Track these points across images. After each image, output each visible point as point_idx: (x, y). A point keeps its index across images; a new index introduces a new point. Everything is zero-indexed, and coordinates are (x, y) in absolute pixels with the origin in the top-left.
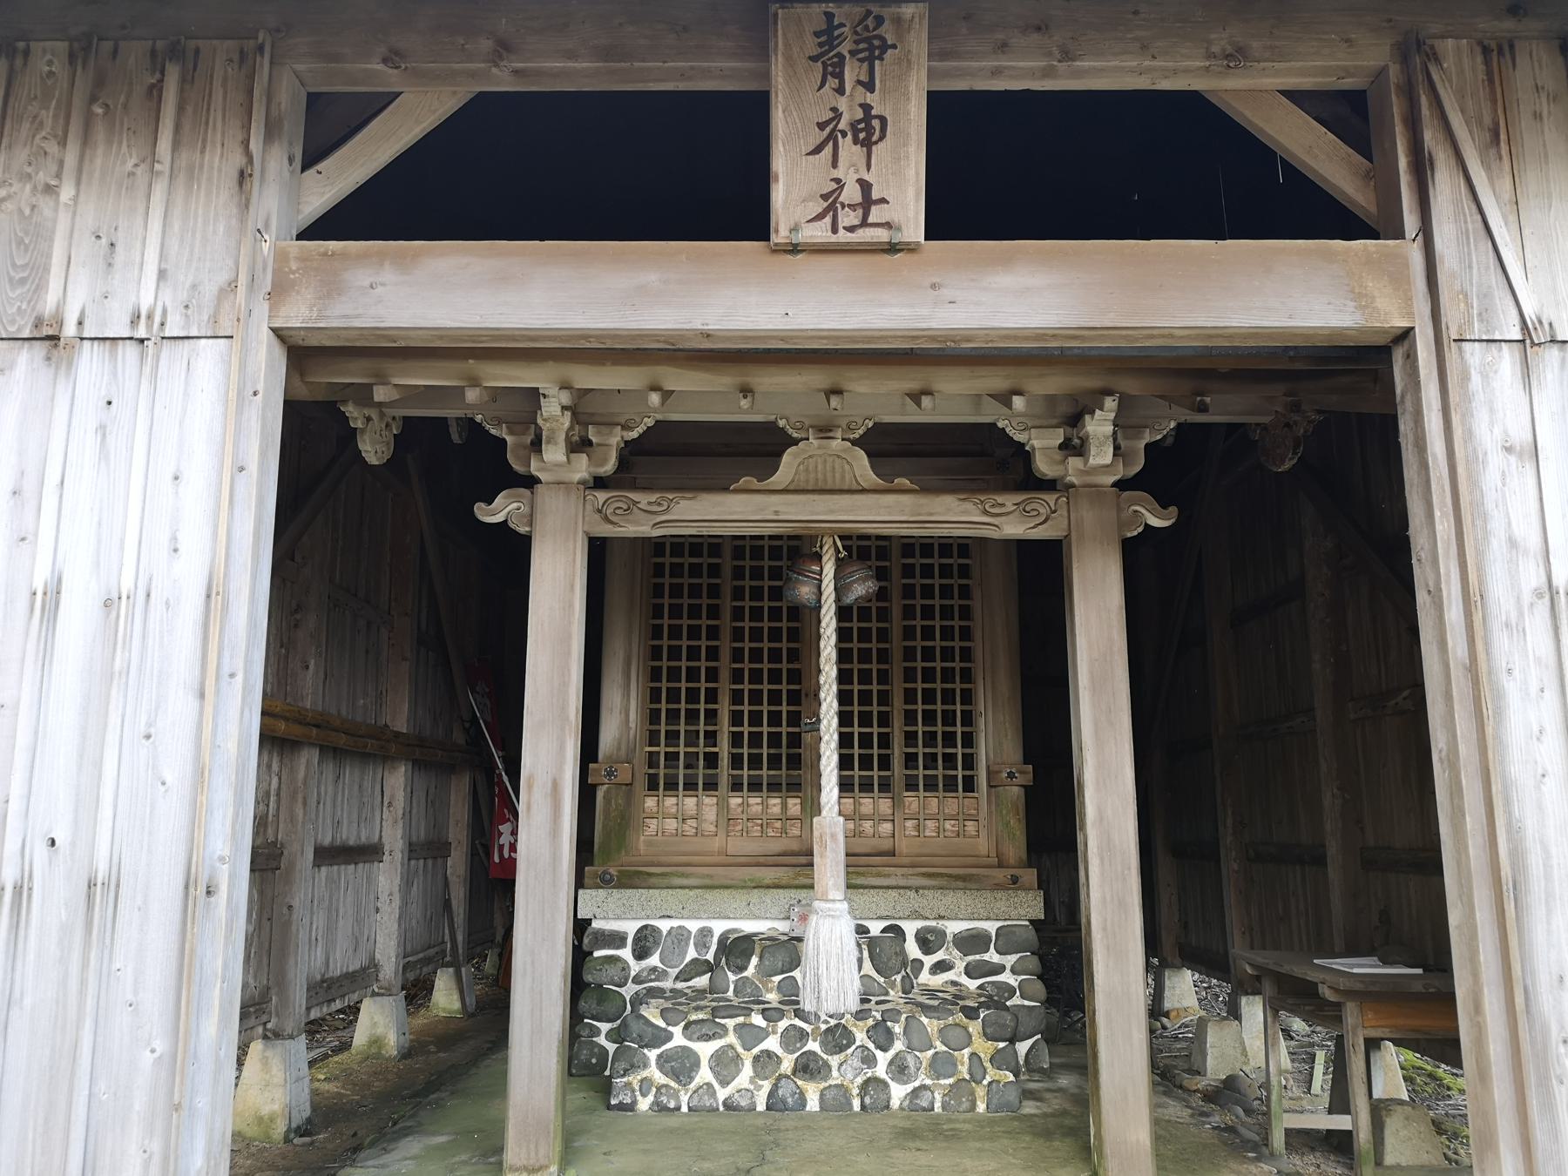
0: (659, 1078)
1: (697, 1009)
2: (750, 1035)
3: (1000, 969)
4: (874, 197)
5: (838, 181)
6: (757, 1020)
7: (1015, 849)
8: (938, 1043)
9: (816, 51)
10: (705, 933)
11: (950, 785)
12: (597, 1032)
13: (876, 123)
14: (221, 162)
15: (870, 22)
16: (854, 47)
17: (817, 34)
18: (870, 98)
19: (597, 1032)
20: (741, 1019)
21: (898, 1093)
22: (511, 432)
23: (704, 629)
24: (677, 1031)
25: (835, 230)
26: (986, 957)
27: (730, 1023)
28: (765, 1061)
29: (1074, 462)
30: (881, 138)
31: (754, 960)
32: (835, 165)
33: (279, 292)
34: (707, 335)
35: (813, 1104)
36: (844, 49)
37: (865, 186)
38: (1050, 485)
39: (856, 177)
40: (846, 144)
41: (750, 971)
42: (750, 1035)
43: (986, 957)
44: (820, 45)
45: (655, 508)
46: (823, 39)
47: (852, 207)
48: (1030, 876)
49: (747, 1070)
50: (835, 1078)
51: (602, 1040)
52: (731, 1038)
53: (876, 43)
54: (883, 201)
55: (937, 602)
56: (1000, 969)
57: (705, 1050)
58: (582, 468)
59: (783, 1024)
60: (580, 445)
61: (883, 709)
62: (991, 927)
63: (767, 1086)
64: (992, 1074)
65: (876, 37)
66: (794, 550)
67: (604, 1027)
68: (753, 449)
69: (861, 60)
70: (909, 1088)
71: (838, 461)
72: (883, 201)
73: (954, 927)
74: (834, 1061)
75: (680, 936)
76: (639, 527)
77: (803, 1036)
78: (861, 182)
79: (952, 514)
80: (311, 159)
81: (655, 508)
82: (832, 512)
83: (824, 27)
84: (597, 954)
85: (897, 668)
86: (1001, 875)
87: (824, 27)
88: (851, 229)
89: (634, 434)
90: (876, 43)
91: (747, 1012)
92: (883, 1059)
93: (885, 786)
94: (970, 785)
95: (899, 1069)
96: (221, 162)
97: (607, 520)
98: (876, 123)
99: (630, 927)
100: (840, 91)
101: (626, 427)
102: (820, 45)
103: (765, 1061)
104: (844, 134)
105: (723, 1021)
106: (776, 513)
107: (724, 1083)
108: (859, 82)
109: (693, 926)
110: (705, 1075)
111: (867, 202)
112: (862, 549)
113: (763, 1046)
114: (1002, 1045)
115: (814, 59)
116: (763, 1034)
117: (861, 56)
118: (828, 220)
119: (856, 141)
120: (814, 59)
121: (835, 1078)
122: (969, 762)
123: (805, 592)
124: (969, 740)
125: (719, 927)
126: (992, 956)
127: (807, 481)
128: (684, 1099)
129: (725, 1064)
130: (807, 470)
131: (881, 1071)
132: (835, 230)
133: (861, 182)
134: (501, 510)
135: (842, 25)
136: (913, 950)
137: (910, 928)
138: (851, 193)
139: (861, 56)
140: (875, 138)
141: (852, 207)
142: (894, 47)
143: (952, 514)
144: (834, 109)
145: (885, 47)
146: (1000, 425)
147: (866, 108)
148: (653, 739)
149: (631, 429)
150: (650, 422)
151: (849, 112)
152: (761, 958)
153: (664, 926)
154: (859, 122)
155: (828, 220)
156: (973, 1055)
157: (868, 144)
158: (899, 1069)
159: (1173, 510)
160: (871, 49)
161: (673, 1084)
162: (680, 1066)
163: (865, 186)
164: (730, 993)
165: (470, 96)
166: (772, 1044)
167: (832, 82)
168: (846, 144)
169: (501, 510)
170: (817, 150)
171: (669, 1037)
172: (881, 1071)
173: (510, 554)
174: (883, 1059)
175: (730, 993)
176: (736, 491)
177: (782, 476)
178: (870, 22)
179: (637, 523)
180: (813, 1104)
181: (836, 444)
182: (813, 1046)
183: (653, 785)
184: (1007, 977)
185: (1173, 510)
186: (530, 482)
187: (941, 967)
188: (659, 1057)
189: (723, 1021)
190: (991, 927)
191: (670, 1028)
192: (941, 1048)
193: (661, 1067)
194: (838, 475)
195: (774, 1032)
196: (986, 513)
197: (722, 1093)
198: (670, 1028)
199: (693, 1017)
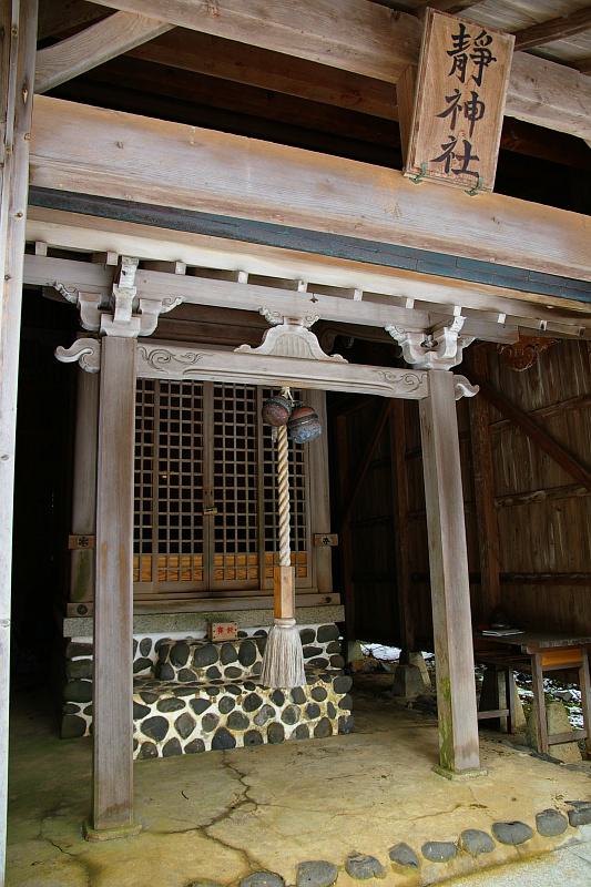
1: (164, 691)
2: (199, 706)
3: (320, 651)
4: (472, 154)
5: (453, 138)
6: (204, 695)
7: (328, 583)
8: (310, 698)
9: (452, 49)
10: (147, 643)
12: (78, 709)
13: (478, 106)
15: (484, 39)
16: (473, 53)
17: (454, 38)
18: (478, 90)
19: (78, 709)
20: (193, 696)
21: (289, 729)
22: (85, 299)
24: (153, 707)
25: (447, 171)
26: (312, 645)
27: (187, 699)
28: (209, 722)
29: (432, 355)
30: (481, 117)
31: (190, 658)
32: (452, 128)
35: (240, 742)
36: (468, 52)
37: (468, 147)
39: (463, 138)
40: (461, 114)
41: (188, 665)
43: (312, 645)
44: (455, 45)
45: (186, 360)
46: (457, 41)
47: (460, 158)
48: (336, 597)
49: (199, 727)
50: (252, 726)
51: (81, 714)
52: (188, 709)
53: (486, 54)
54: (476, 158)
55: (181, 461)
56: (320, 651)
57: (172, 717)
59: (219, 697)
60: (136, 312)
61: (147, 513)
62: (315, 627)
63: (211, 735)
64: (340, 713)
65: (486, 50)
67: (83, 706)
68: (248, 328)
69: (476, 63)
70: (295, 726)
71: (300, 340)
72: (476, 158)
74: (250, 715)
77: (232, 702)
78: (465, 142)
81: (186, 360)
82: (298, 372)
83: (458, 34)
84: (74, 659)
85: (209, 485)
86: (320, 598)
87: (458, 34)
88: (456, 172)
89: (168, 309)
90: (486, 54)
91: (197, 691)
92: (279, 711)
97: (152, 365)
98: (478, 106)
100: (462, 79)
101: (164, 304)
102: (455, 45)
104: (460, 110)
105: (182, 698)
106: (265, 369)
107: (185, 737)
108: (474, 77)
110: (172, 733)
111: (467, 157)
113: (208, 711)
114: (344, 695)
115: (451, 53)
116: (207, 704)
117: (476, 60)
118: (444, 162)
119: (466, 115)
120: (451, 53)
121: (252, 726)
125: (155, 638)
126: (316, 644)
127: (282, 351)
128: (160, 748)
130: (281, 343)
131: (278, 718)
132: (447, 171)
133: (465, 142)
135: (468, 36)
138: (459, 149)
139: (476, 60)
140: (477, 116)
141: (460, 158)
142: (495, 60)
144: (457, 91)
145: (490, 58)
146: (387, 329)
147: (475, 95)
149: (169, 305)
150: (179, 302)
151: (466, 97)
152: (195, 657)
154: (469, 103)
155: (444, 162)
156: (329, 704)
157: (473, 119)
158: (289, 716)
159: (477, 387)
160: (483, 57)
161: (152, 741)
163: (468, 147)
164: (176, 679)
165: (169, 28)
167: (458, 72)
168: (461, 114)
170: (444, 115)
171: (149, 710)
172: (278, 718)
174: (279, 711)
175: (176, 679)
176: (237, 353)
177: (265, 348)
178: (484, 39)
179: (174, 369)
180: (240, 742)
181: (299, 329)
182: (238, 708)
184: (325, 655)
185: (477, 387)
188: (143, 725)
189: (182, 698)
190: (315, 627)
191: (149, 706)
192: (312, 701)
193: (142, 730)
194: (300, 349)
195: (215, 702)
196: (386, 380)
197: (184, 743)
198: (149, 706)
199: (163, 697)
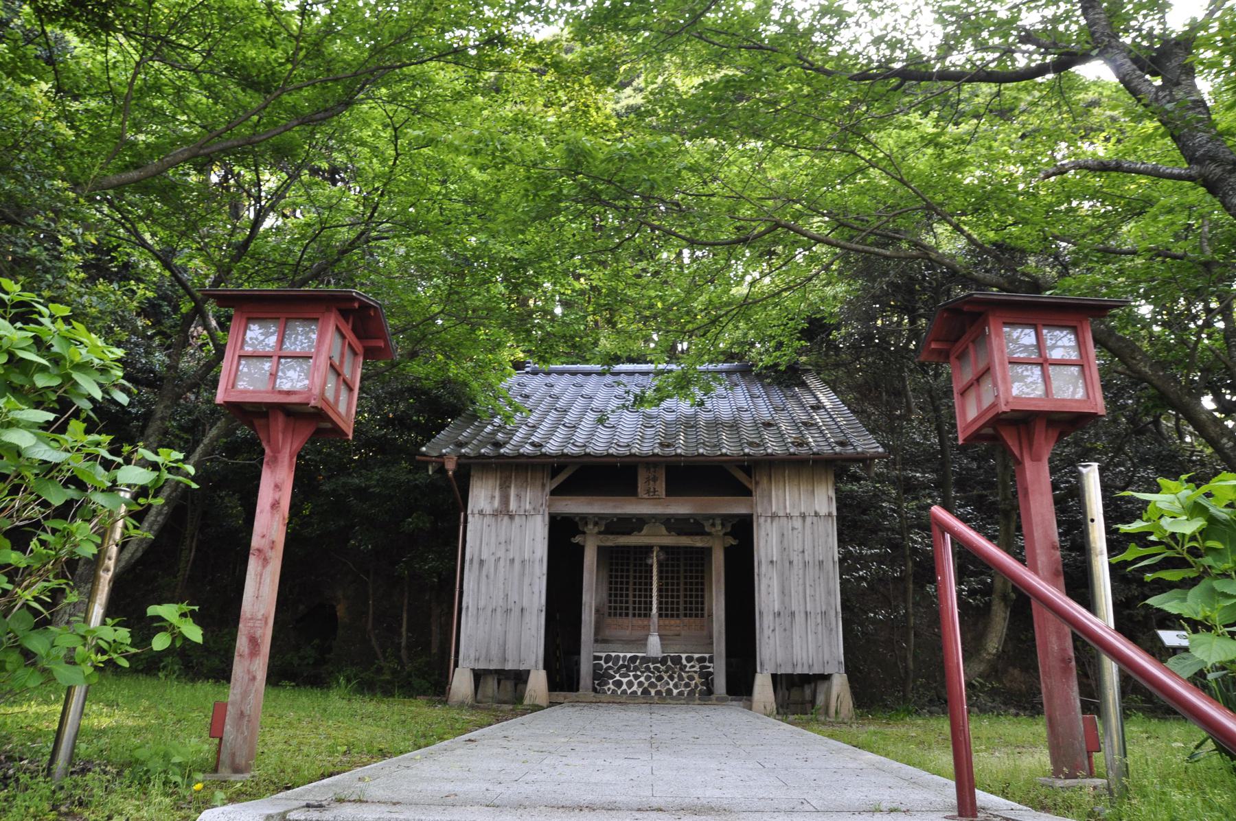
0: (612, 687)
2: (636, 677)
11: (697, 616)
14: (539, 483)
23: (624, 566)
28: (640, 684)
33: (549, 506)
34: (654, 744)
38: (709, 534)
42: (636, 677)
57: (625, 680)
58: (596, 530)
66: (648, 549)
73: (696, 656)
75: (618, 657)
76: (609, 544)
79: (685, 541)
80: (552, 478)
92: (671, 683)
93: (678, 616)
94: (702, 616)
95: (676, 686)
96: (539, 483)
99: (603, 655)
103: (640, 684)
109: (621, 655)
110: (624, 687)
112: (663, 548)
122: (702, 609)
123: (649, 562)
124: (703, 603)
129: (630, 684)
131: (671, 686)
134: (577, 539)
136: (684, 662)
137: (684, 656)
143: (685, 541)
148: (610, 602)
153: (613, 654)
158: (676, 686)
162: (618, 684)
166: (642, 679)
169: (577, 539)
172: (671, 686)
173: (580, 550)
174: (671, 683)
177: (644, 532)
183: (610, 614)
186: (584, 533)
187: (693, 667)
